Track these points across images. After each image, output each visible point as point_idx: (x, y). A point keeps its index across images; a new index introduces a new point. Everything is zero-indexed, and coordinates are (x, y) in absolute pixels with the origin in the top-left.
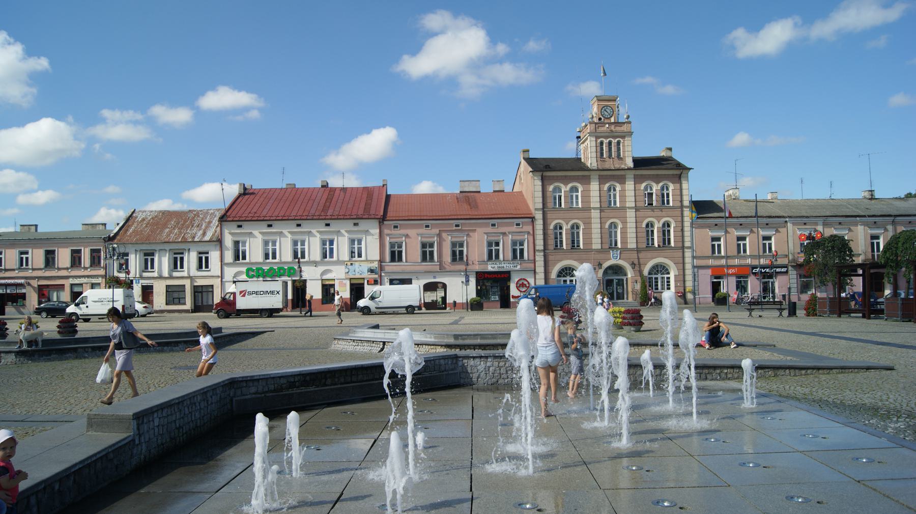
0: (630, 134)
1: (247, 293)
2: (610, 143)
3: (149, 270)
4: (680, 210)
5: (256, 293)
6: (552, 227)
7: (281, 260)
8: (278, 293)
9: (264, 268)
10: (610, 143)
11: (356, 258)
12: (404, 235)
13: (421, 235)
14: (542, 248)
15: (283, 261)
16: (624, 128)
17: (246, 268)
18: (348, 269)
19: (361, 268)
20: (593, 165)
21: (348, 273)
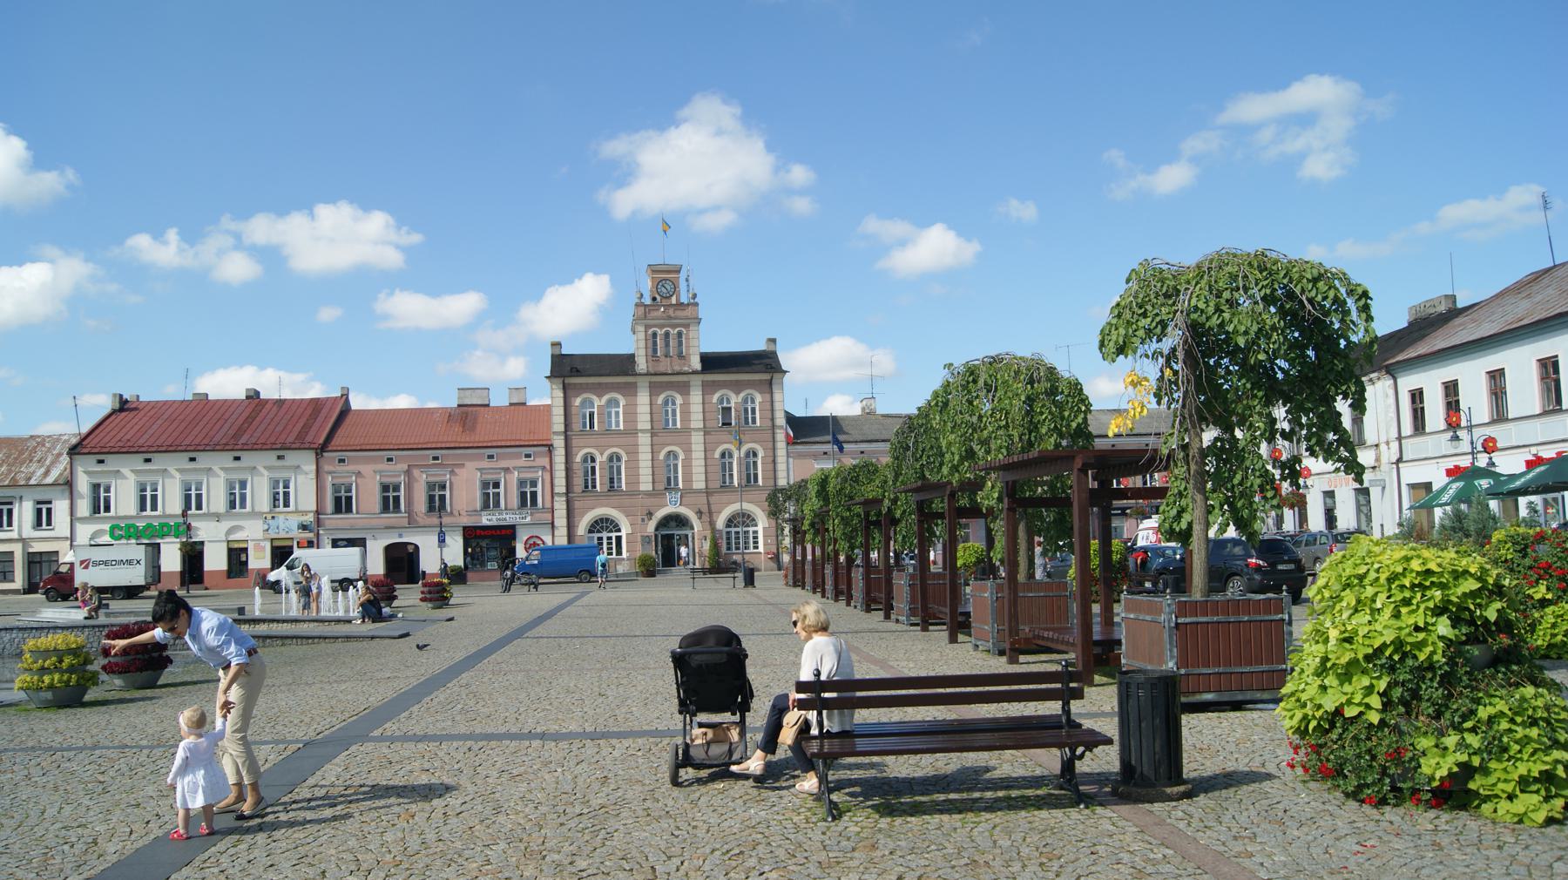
3: (44, 526)
5: (105, 563)
8: (138, 562)
11: (281, 508)
14: (563, 490)
19: (287, 523)
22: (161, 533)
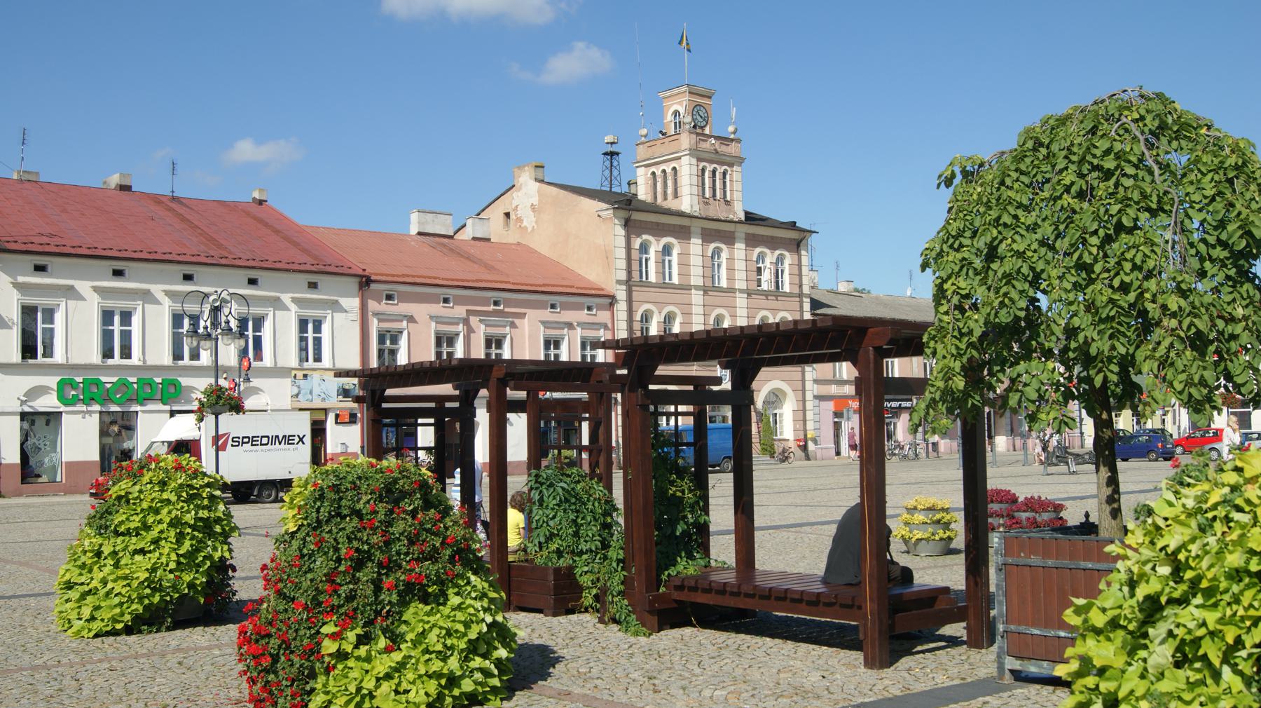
0: (739, 161)
1: (230, 442)
2: (714, 172)
4: (798, 299)
5: (252, 440)
6: (638, 318)
7: (144, 361)
8: (301, 440)
9: (104, 379)
10: (714, 172)
11: (311, 363)
12: (405, 316)
13: (438, 319)
15: (149, 363)
16: (733, 149)
17: (59, 378)
18: (299, 387)
19: (323, 386)
21: (297, 395)
22: (142, 395)
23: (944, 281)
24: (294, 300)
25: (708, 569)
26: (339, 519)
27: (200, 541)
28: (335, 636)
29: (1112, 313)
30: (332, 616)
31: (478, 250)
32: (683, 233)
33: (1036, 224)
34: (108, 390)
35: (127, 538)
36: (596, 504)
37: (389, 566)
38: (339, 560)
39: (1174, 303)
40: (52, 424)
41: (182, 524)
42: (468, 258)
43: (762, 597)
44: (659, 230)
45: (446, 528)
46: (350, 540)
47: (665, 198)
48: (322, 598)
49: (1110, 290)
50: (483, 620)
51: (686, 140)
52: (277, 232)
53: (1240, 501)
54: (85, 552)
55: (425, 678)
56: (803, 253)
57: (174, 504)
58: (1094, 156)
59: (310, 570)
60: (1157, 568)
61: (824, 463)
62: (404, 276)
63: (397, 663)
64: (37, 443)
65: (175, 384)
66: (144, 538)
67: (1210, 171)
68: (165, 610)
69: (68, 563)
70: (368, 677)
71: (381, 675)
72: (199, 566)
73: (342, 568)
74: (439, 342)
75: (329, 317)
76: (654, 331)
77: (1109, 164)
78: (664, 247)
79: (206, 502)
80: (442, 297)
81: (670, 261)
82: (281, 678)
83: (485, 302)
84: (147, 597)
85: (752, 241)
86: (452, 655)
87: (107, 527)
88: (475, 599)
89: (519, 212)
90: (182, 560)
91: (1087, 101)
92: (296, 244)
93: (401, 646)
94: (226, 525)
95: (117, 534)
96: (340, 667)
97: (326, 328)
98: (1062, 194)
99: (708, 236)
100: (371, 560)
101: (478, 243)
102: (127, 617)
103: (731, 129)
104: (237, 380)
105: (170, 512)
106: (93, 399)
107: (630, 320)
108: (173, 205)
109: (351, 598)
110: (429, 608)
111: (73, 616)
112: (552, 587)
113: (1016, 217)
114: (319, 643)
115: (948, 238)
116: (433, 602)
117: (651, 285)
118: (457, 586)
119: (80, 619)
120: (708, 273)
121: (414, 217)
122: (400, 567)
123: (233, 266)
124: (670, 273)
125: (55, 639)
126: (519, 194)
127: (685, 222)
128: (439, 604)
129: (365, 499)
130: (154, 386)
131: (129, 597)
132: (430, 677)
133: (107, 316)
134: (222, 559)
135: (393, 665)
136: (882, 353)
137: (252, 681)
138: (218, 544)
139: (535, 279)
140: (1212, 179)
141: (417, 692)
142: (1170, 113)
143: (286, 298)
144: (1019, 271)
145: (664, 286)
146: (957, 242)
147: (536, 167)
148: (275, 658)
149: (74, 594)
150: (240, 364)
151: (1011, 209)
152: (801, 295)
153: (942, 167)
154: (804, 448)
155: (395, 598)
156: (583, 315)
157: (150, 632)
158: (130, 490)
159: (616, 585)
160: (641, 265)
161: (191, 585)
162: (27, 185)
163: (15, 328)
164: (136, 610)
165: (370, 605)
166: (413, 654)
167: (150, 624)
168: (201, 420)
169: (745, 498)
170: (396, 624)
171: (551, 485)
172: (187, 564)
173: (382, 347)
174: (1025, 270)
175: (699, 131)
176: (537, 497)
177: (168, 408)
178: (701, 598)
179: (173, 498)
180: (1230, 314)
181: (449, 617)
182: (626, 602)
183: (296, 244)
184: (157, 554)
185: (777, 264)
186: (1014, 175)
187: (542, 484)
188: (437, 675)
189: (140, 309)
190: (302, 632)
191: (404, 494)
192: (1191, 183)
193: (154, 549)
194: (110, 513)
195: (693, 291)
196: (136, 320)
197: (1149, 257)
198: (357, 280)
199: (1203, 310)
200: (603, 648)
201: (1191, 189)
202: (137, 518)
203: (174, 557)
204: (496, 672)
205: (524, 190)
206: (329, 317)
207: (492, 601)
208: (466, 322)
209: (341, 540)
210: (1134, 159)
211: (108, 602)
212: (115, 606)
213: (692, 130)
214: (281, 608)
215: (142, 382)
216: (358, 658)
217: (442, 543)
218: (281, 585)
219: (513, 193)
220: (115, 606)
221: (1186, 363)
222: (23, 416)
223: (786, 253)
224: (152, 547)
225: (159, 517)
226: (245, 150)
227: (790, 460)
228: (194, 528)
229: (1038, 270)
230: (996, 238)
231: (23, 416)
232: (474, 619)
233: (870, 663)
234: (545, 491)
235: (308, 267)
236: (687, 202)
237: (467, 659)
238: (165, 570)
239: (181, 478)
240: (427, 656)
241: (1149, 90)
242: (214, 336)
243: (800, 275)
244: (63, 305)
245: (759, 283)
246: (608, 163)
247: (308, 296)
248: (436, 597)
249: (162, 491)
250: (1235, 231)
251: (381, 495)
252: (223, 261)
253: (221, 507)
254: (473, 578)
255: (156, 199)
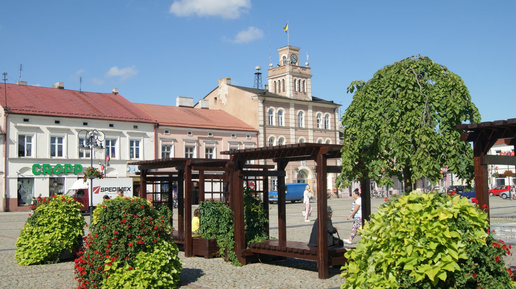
1: (100, 190)
2: (299, 81)
4: (334, 133)
6: (268, 140)
7: (67, 157)
8: (129, 189)
9: (51, 165)
10: (299, 81)
12: (173, 139)
13: (186, 141)
16: (307, 72)
18: (130, 168)
20: (291, 96)
21: (129, 171)
22: (66, 171)
23: (347, 129)
24: (128, 133)
25: (268, 240)
26: (112, 220)
27: (71, 229)
28: (109, 264)
29: (403, 142)
30: (109, 256)
31: (204, 113)
32: (287, 106)
33: (378, 107)
34: (53, 169)
35: (43, 227)
36: (227, 215)
37: (131, 237)
38: (112, 235)
39: (425, 138)
40: (30, 182)
41: (64, 222)
42: (199, 116)
43: (273, 250)
44: (277, 105)
45: (155, 223)
46: (116, 227)
47: (280, 92)
48: (105, 249)
49: (403, 133)
50: (168, 259)
51: (288, 68)
52: (122, 105)
53: (398, 213)
54: (26, 232)
55: (143, 280)
56: (336, 114)
57: (61, 214)
58: (399, 82)
59: (101, 239)
60: (373, 238)
61: (345, 199)
62: (172, 123)
63: (133, 274)
64: (24, 190)
65: (79, 167)
66: (49, 227)
67: (442, 87)
68: (57, 255)
69: (20, 236)
70: (121, 279)
71: (126, 279)
72: (70, 238)
73: (113, 238)
74: (187, 150)
75: (142, 140)
76: (275, 144)
77: (403, 85)
78: (279, 111)
79: (74, 213)
80: (188, 132)
81: (281, 117)
82: (90, 280)
83: (205, 134)
84: (50, 250)
85: (315, 109)
86: (154, 271)
87: (35, 223)
88: (165, 250)
89: (221, 98)
90: (64, 236)
91: (399, 61)
92: (129, 111)
93: (136, 268)
94: (82, 222)
95: (39, 225)
96: (111, 275)
97: (141, 144)
98: (387, 96)
99: (297, 107)
100: (124, 235)
101: (204, 110)
102: (42, 258)
103: (307, 63)
104: (104, 165)
105: (59, 217)
106: (46, 173)
107: (265, 141)
108: (80, 95)
109: (116, 249)
110: (146, 253)
111: (21, 257)
112: (208, 247)
113: (370, 104)
114: (104, 267)
115: (349, 112)
116: (148, 251)
117: (273, 127)
118: (159, 246)
119: (24, 258)
120: (297, 122)
121: (178, 99)
122: (135, 238)
123: (103, 119)
124: (281, 122)
125: (14, 266)
126: (221, 90)
127: (288, 101)
128: (151, 252)
129: (123, 212)
130: (71, 167)
131: (43, 250)
132: (145, 279)
133: (53, 139)
134: (80, 235)
135: (131, 275)
136: (326, 157)
137: (80, 281)
138: (78, 230)
139: (226, 124)
140: (443, 91)
141: (140, 285)
142: (430, 65)
143: (125, 132)
144: (371, 125)
145: (279, 127)
146: (352, 114)
147: (228, 79)
148: (88, 272)
149: (22, 249)
150: (105, 158)
151: (369, 102)
152: (335, 131)
153: (348, 85)
154: (337, 193)
155: (133, 250)
156: (245, 139)
157: (51, 263)
158: (44, 209)
159: (230, 246)
160: (269, 119)
161: (67, 246)
162: (22, 87)
163: (16, 144)
164: (45, 255)
165: (124, 252)
166: (139, 271)
167: (51, 261)
168: (85, 181)
169: (282, 213)
170: (134, 259)
171: (208, 208)
172: (65, 237)
173: (163, 152)
174: (373, 125)
175: (293, 64)
176: (202, 212)
177: (77, 176)
178: (262, 252)
179: (61, 212)
180: (448, 143)
181: (154, 257)
182: (234, 253)
183: (129, 111)
184: (54, 233)
185: (325, 118)
186: (371, 89)
187: (204, 207)
188: (148, 279)
189: (66, 136)
190: (98, 263)
191: (138, 210)
192: (435, 92)
193: (53, 231)
194: (36, 217)
195: (291, 129)
196: (64, 141)
197: (417, 121)
198: (154, 125)
199: (435, 141)
200: (222, 271)
201: (435, 94)
202: (46, 219)
203: (60, 235)
204: (172, 278)
205: (222, 89)
206: (142, 140)
207: (172, 251)
208: (198, 142)
209: (113, 228)
210: (413, 83)
211: (35, 252)
212: (37, 253)
213: (290, 64)
214: (91, 253)
215: (44, 166)
216: (118, 272)
217: (153, 229)
218: (91, 245)
219: (218, 90)
220: (37, 253)
221: (428, 161)
222: (19, 179)
223: (329, 114)
224: (52, 231)
225: (55, 219)
226: (114, 71)
227: (331, 198)
228: (68, 223)
229: (378, 125)
230: (364, 112)
231: (19, 179)
232: (164, 258)
233: (320, 277)
234: (205, 210)
235: (134, 120)
236: (288, 93)
237: (160, 273)
238: (57, 240)
239: (64, 204)
240: (145, 272)
241: (423, 56)
242: (91, 148)
243: (335, 123)
244: (35, 135)
245: (318, 126)
246: (257, 78)
247: (134, 131)
248: (150, 249)
249: (57, 209)
250: (449, 111)
251: (129, 211)
252: (100, 117)
253: (80, 215)
254: (165, 242)
255: (73, 92)
